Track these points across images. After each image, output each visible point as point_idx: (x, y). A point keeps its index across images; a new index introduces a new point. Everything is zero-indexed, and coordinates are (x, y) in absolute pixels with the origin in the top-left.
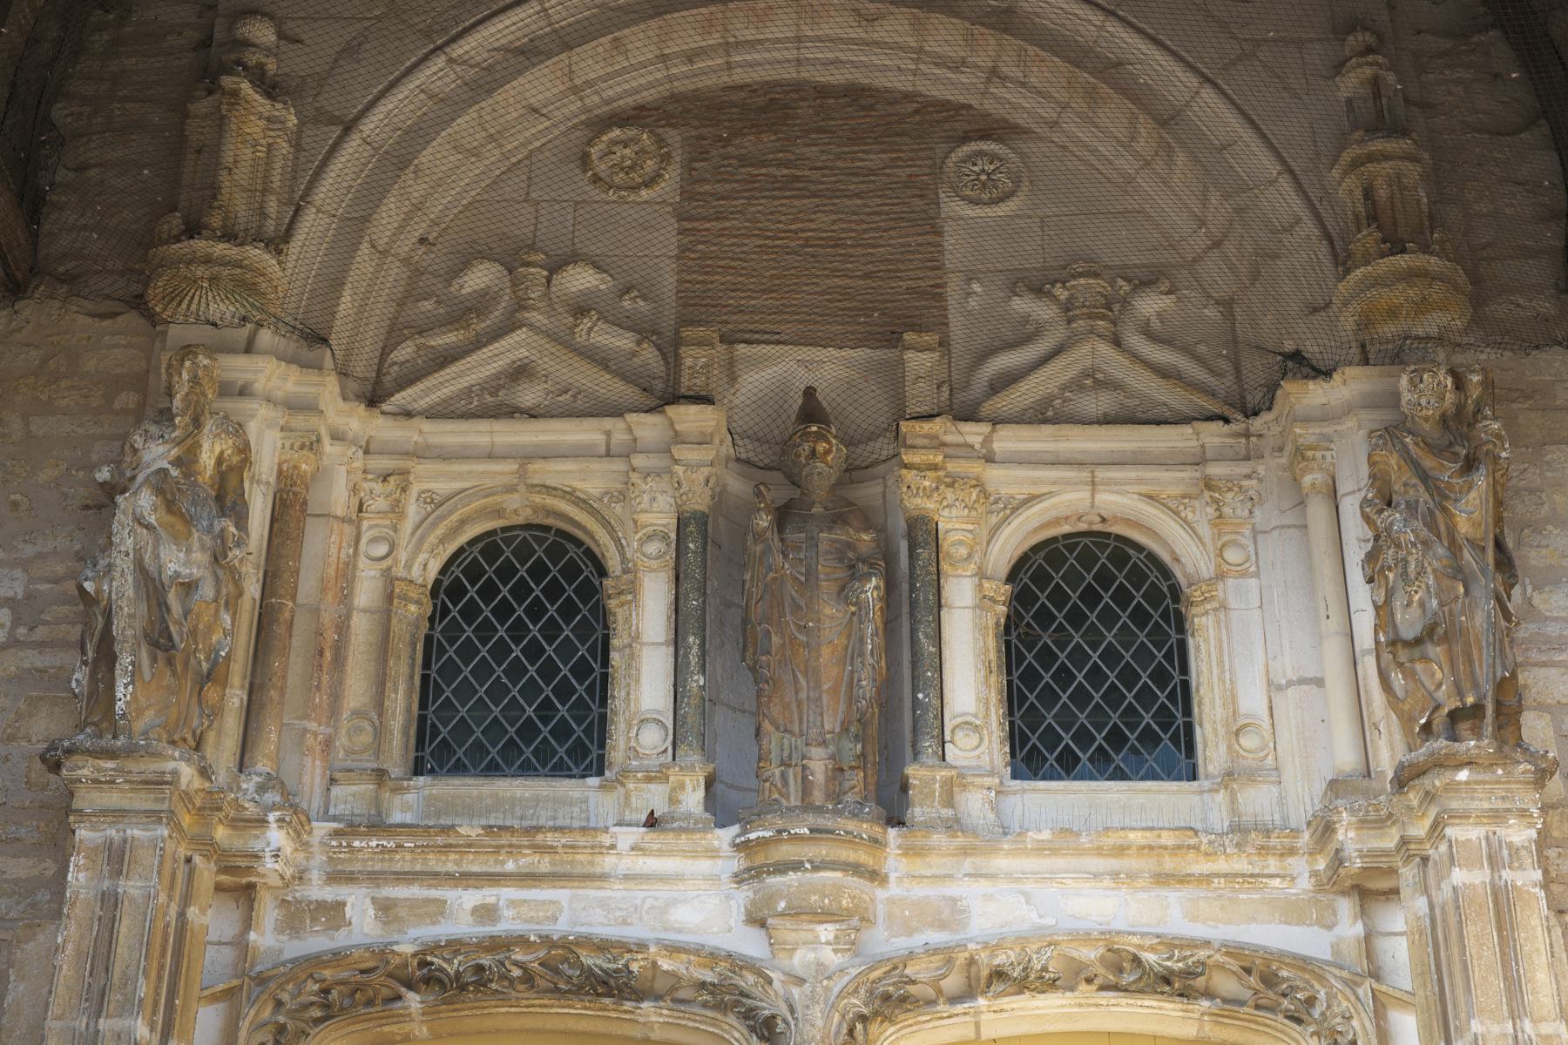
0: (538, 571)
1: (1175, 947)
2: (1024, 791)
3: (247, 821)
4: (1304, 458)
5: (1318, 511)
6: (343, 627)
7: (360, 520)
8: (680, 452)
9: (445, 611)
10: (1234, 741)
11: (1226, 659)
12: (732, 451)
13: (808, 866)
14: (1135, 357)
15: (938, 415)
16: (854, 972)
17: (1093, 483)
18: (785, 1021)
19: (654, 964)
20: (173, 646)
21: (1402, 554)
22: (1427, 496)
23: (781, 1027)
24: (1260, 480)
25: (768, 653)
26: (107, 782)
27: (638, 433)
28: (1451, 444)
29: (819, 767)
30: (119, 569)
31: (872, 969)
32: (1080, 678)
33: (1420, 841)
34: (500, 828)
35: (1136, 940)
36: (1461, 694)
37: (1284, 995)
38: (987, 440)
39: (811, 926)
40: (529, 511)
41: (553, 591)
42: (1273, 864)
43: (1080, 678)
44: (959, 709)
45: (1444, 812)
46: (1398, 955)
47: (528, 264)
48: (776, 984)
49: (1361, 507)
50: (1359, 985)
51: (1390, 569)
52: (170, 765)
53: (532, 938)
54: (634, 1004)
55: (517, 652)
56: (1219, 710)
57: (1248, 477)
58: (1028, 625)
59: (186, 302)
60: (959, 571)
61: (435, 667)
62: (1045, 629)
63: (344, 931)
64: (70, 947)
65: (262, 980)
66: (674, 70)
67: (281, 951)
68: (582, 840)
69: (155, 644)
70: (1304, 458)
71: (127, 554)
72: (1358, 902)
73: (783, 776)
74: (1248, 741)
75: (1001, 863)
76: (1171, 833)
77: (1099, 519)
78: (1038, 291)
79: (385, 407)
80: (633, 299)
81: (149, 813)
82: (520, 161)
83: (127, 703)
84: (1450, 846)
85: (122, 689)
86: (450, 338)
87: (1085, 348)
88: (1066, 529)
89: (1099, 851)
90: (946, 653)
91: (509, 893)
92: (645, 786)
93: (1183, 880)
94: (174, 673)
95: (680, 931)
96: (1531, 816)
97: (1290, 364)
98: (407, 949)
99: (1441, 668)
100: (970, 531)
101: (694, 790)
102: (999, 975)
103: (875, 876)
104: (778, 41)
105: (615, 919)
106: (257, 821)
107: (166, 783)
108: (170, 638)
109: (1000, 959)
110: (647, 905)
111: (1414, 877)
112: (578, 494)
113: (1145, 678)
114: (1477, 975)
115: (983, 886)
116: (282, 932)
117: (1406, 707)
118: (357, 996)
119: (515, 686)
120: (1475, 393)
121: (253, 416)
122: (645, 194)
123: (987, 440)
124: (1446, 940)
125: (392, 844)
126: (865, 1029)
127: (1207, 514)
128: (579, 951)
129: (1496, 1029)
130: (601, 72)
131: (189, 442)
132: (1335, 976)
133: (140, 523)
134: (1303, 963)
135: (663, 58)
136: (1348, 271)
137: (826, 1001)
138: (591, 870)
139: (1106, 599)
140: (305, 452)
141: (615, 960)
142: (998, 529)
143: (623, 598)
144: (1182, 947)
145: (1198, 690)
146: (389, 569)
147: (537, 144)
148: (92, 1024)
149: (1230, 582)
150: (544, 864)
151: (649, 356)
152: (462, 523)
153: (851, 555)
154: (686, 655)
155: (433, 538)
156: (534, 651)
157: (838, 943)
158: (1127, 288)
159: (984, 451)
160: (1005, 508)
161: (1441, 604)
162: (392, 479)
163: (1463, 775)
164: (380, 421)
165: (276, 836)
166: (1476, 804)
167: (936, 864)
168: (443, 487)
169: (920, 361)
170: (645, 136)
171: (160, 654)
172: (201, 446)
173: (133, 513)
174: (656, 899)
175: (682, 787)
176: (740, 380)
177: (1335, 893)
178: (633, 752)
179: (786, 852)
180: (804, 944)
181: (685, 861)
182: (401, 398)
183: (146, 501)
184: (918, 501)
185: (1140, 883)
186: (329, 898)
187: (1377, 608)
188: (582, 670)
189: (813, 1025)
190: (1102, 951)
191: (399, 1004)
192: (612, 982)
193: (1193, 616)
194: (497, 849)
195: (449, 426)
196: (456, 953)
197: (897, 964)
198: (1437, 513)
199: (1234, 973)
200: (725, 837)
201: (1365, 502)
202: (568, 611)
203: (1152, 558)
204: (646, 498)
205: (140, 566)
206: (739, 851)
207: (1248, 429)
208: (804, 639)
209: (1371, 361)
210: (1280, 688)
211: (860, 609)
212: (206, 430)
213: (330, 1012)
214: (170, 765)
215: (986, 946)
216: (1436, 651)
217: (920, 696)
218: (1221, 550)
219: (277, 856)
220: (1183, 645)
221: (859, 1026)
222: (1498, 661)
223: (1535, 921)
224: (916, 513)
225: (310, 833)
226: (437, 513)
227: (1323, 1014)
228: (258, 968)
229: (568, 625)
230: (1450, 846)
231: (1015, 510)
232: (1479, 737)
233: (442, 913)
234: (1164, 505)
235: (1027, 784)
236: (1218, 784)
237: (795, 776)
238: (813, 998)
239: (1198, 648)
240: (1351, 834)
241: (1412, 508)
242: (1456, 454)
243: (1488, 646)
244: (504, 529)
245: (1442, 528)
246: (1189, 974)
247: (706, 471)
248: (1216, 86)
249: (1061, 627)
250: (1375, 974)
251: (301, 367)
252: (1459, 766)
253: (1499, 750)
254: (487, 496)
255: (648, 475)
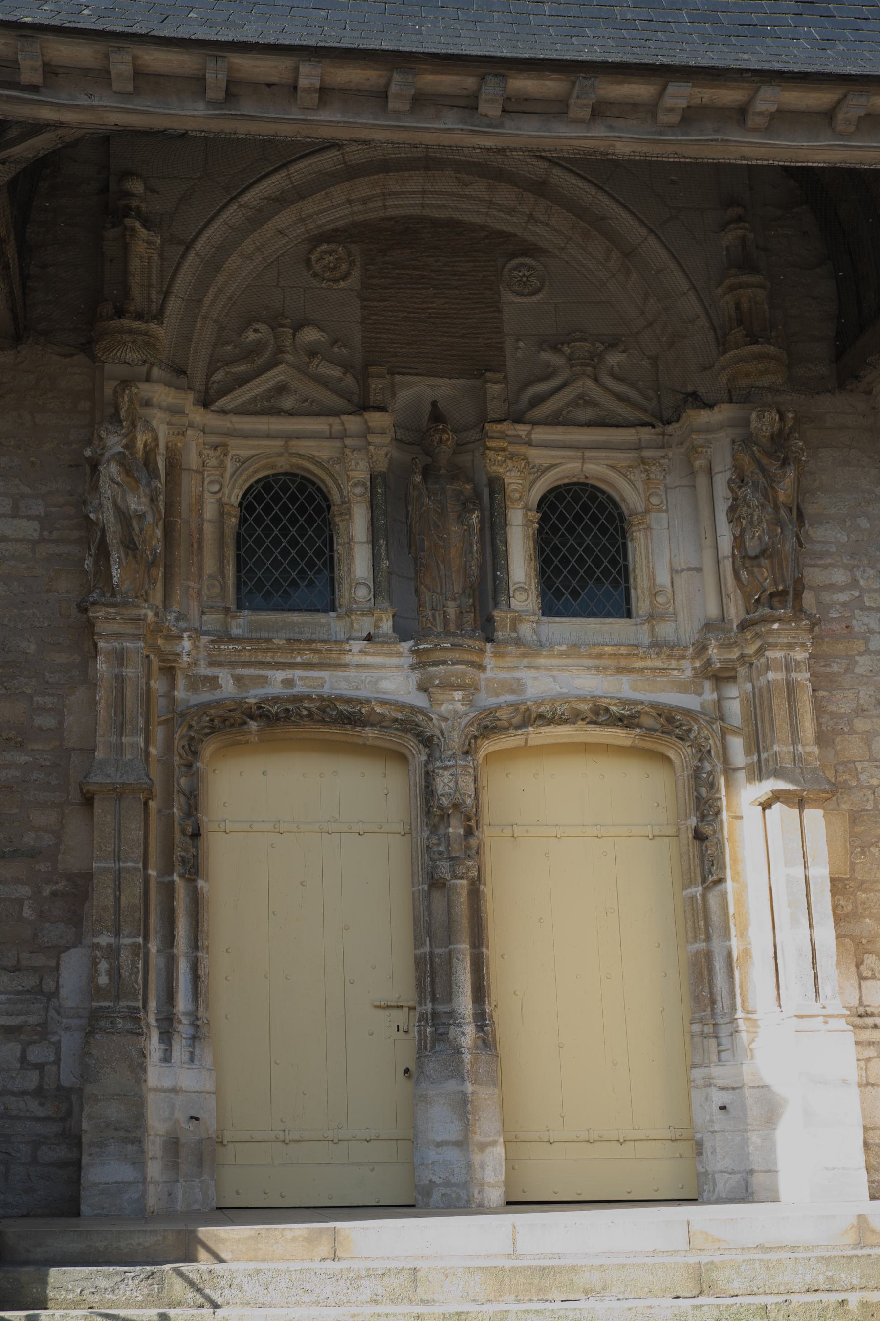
0: (293, 499)
1: (627, 704)
2: (549, 623)
3: (171, 636)
4: (697, 452)
5: (702, 481)
6: (201, 531)
7: (204, 471)
8: (371, 438)
9: (246, 520)
10: (653, 599)
11: (650, 556)
12: (393, 435)
13: (450, 663)
14: (607, 389)
15: (505, 420)
16: (472, 715)
17: (583, 458)
18: (438, 738)
19: (373, 709)
20: (137, 549)
21: (750, 511)
22: (763, 479)
23: (436, 741)
24: (670, 460)
25: (423, 551)
26: (112, 619)
27: (347, 426)
28: (776, 451)
29: (452, 610)
30: (106, 507)
31: (481, 714)
32: (573, 562)
33: (750, 656)
34: (294, 640)
35: (607, 701)
36: (776, 585)
37: (677, 727)
38: (529, 433)
39: (451, 692)
40: (288, 466)
41: (302, 510)
42: (674, 664)
43: (573, 562)
44: (516, 580)
45: (766, 644)
46: (734, 709)
47: (283, 326)
48: (434, 721)
49: (729, 483)
50: (714, 723)
51: (744, 518)
52: (143, 611)
53: (314, 696)
54: (361, 728)
55: (285, 543)
56: (646, 582)
57: (663, 457)
58: (547, 533)
59: (115, 351)
60: (515, 506)
61: (243, 550)
62: (555, 536)
63: (218, 691)
64: (103, 701)
65: (182, 715)
66: (355, 209)
67: (188, 701)
68: (335, 647)
69: (127, 547)
70: (697, 452)
71: (109, 499)
72: (715, 683)
73: (433, 616)
74: (660, 599)
75: (541, 661)
76: (625, 648)
77: (584, 477)
78: (555, 348)
79: (212, 408)
80: (339, 347)
81: (134, 635)
82: (272, 262)
83: (118, 578)
84: (767, 661)
85: (115, 571)
86: (241, 368)
87: (580, 383)
88: (566, 481)
89: (590, 656)
90: (510, 550)
91: (299, 673)
92: (360, 618)
93: (630, 671)
94: (137, 562)
95: (384, 693)
96: (807, 646)
97: (691, 399)
98: (253, 701)
99: (767, 571)
100: (521, 484)
101: (387, 621)
102: (541, 716)
103: (481, 667)
104: (414, 193)
105: (353, 687)
106: (178, 636)
107: (141, 620)
108: (135, 544)
109: (542, 709)
110: (368, 680)
111: (745, 673)
112: (316, 458)
113: (606, 563)
114: (777, 723)
115: (533, 673)
116: (188, 691)
117: (748, 589)
118: (227, 723)
119: (285, 561)
120: (790, 423)
121: (155, 417)
122: (342, 284)
123: (529, 433)
124: (761, 705)
125: (240, 647)
126: (475, 742)
127: (642, 478)
128: (336, 703)
129: (785, 749)
130: (316, 209)
131: (131, 435)
132: (703, 719)
133: (113, 482)
134: (687, 712)
135: (349, 201)
136: (725, 352)
137: (459, 729)
138: (339, 662)
139: (586, 520)
140: (180, 437)
141: (354, 708)
142: (534, 483)
143: (343, 517)
144: (629, 704)
145: (634, 571)
146: (221, 499)
147: (281, 252)
148: (118, 740)
149: (653, 514)
150: (315, 658)
151: (350, 381)
152: (255, 472)
153: (462, 497)
154: (379, 550)
155: (240, 481)
156: (294, 543)
157: (464, 701)
158: (602, 348)
159: (527, 439)
160: (538, 471)
161: (769, 538)
162: (218, 449)
163: (776, 626)
164: (210, 416)
165: (187, 644)
166: (780, 640)
167: (509, 661)
168: (245, 453)
169: (494, 389)
170: (340, 249)
171: (130, 552)
172: (137, 438)
173: (109, 476)
174: (372, 677)
175: (381, 620)
176: (397, 396)
177: (703, 678)
178: (353, 600)
179: (438, 655)
180: (447, 701)
181: (386, 658)
182: (221, 403)
183: (114, 468)
184: (495, 468)
185: (609, 672)
186: (210, 674)
187: (735, 538)
188: (319, 553)
189: (454, 741)
190: (591, 705)
191: (246, 727)
192: (352, 718)
193: (633, 532)
194: (292, 651)
195: (246, 419)
196: (276, 703)
197: (492, 711)
198: (769, 489)
199: (654, 717)
200: (406, 646)
201: (730, 481)
202: (310, 521)
203: (610, 497)
204: (353, 463)
205: (115, 503)
206: (413, 654)
207: (664, 432)
208: (442, 544)
209: (734, 401)
210: (677, 572)
211: (469, 528)
212: (138, 429)
213: (213, 730)
214: (143, 611)
215: (536, 702)
216: (765, 562)
217: (498, 573)
218: (649, 497)
219: (189, 654)
220: (625, 545)
221: (473, 741)
222: (796, 569)
223: (805, 698)
224: (494, 474)
225: (199, 641)
226: (242, 468)
227: (696, 737)
228: (180, 709)
229: (310, 529)
230: (767, 661)
231: (543, 472)
232: (784, 608)
233: (266, 682)
234: (619, 471)
235: (550, 619)
236: (645, 621)
237: (439, 616)
238: (453, 728)
239: (635, 549)
240: (715, 651)
241: (755, 486)
242: (778, 457)
243: (792, 562)
244: (274, 475)
245: (771, 497)
246: (632, 717)
247: (385, 449)
248: (656, 235)
249: (563, 535)
250: (721, 718)
251: (176, 389)
252: (774, 622)
253: (795, 614)
254: (267, 458)
255: (354, 450)
